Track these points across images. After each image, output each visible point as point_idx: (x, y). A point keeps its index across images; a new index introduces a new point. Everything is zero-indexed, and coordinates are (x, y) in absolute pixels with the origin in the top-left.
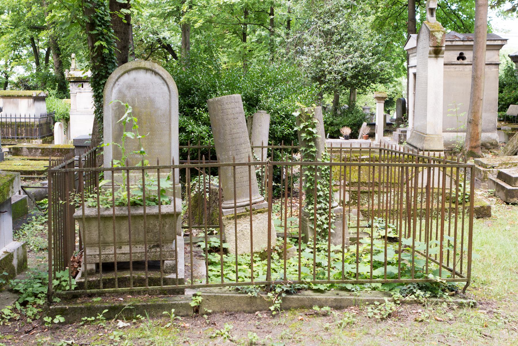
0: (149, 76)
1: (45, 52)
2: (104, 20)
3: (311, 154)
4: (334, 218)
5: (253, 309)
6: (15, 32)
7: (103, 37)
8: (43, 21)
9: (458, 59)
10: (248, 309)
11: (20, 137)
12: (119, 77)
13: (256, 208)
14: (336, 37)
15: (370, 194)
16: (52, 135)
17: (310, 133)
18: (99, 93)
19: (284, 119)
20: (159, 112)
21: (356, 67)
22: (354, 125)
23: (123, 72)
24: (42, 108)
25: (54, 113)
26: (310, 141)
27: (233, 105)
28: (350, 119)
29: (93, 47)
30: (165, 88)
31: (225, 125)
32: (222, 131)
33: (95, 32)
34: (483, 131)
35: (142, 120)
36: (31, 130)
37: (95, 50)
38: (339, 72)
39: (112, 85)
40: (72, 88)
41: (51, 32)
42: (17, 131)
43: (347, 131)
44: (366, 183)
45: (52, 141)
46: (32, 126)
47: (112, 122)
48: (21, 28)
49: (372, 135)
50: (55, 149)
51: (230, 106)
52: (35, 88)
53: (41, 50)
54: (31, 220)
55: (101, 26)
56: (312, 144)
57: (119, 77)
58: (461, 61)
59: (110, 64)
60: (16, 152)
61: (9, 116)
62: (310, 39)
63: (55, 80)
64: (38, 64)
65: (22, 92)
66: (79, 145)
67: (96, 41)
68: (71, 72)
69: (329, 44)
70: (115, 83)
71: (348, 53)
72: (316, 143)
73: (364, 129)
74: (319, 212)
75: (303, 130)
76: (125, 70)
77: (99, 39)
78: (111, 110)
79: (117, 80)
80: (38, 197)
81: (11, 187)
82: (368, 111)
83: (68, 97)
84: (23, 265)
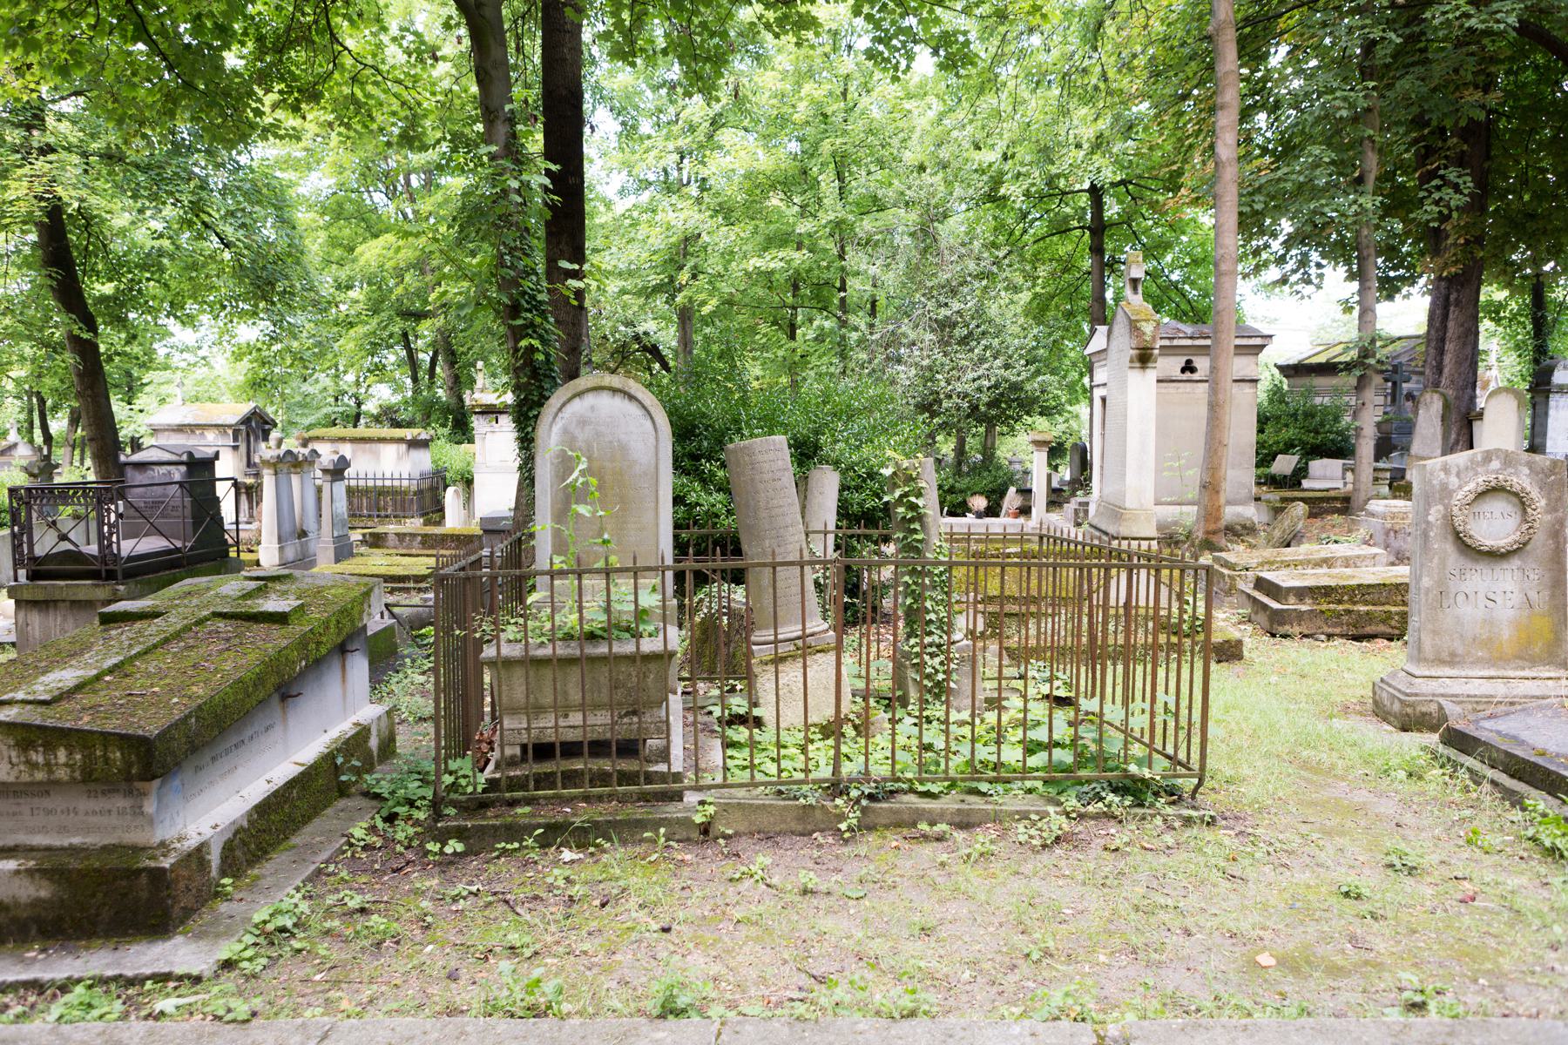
0: (619, 403)
6: (374, 322)
8: (426, 302)
9: (1183, 371)
10: (800, 828)
12: (564, 405)
14: (960, 332)
15: (1022, 618)
16: (442, 510)
17: (913, 507)
19: (864, 481)
21: (996, 386)
22: (993, 491)
24: (422, 461)
25: (446, 470)
26: (912, 520)
27: (771, 456)
28: (986, 481)
29: (516, 350)
30: (649, 424)
31: (757, 492)
33: (519, 322)
34: (1229, 503)
36: (403, 501)
38: (966, 395)
40: (478, 424)
41: (440, 321)
42: (378, 503)
43: (979, 503)
44: (1015, 599)
45: (441, 521)
49: (1025, 511)
51: (766, 457)
52: (410, 424)
53: (421, 356)
54: (403, 665)
56: (917, 526)
57: (564, 405)
58: (1188, 375)
60: (376, 541)
62: (912, 335)
63: (446, 410)
64: (415, 379)
67: (522, 338)
69: (948, 344)
71: (982, 360)
73: (1012, 499)
74: (929, 650)
75: (899, 501)
77: (528, 335)
79: (560, 409)
82: (1017, 467)
83: (471, 441)
84: (388, 748)
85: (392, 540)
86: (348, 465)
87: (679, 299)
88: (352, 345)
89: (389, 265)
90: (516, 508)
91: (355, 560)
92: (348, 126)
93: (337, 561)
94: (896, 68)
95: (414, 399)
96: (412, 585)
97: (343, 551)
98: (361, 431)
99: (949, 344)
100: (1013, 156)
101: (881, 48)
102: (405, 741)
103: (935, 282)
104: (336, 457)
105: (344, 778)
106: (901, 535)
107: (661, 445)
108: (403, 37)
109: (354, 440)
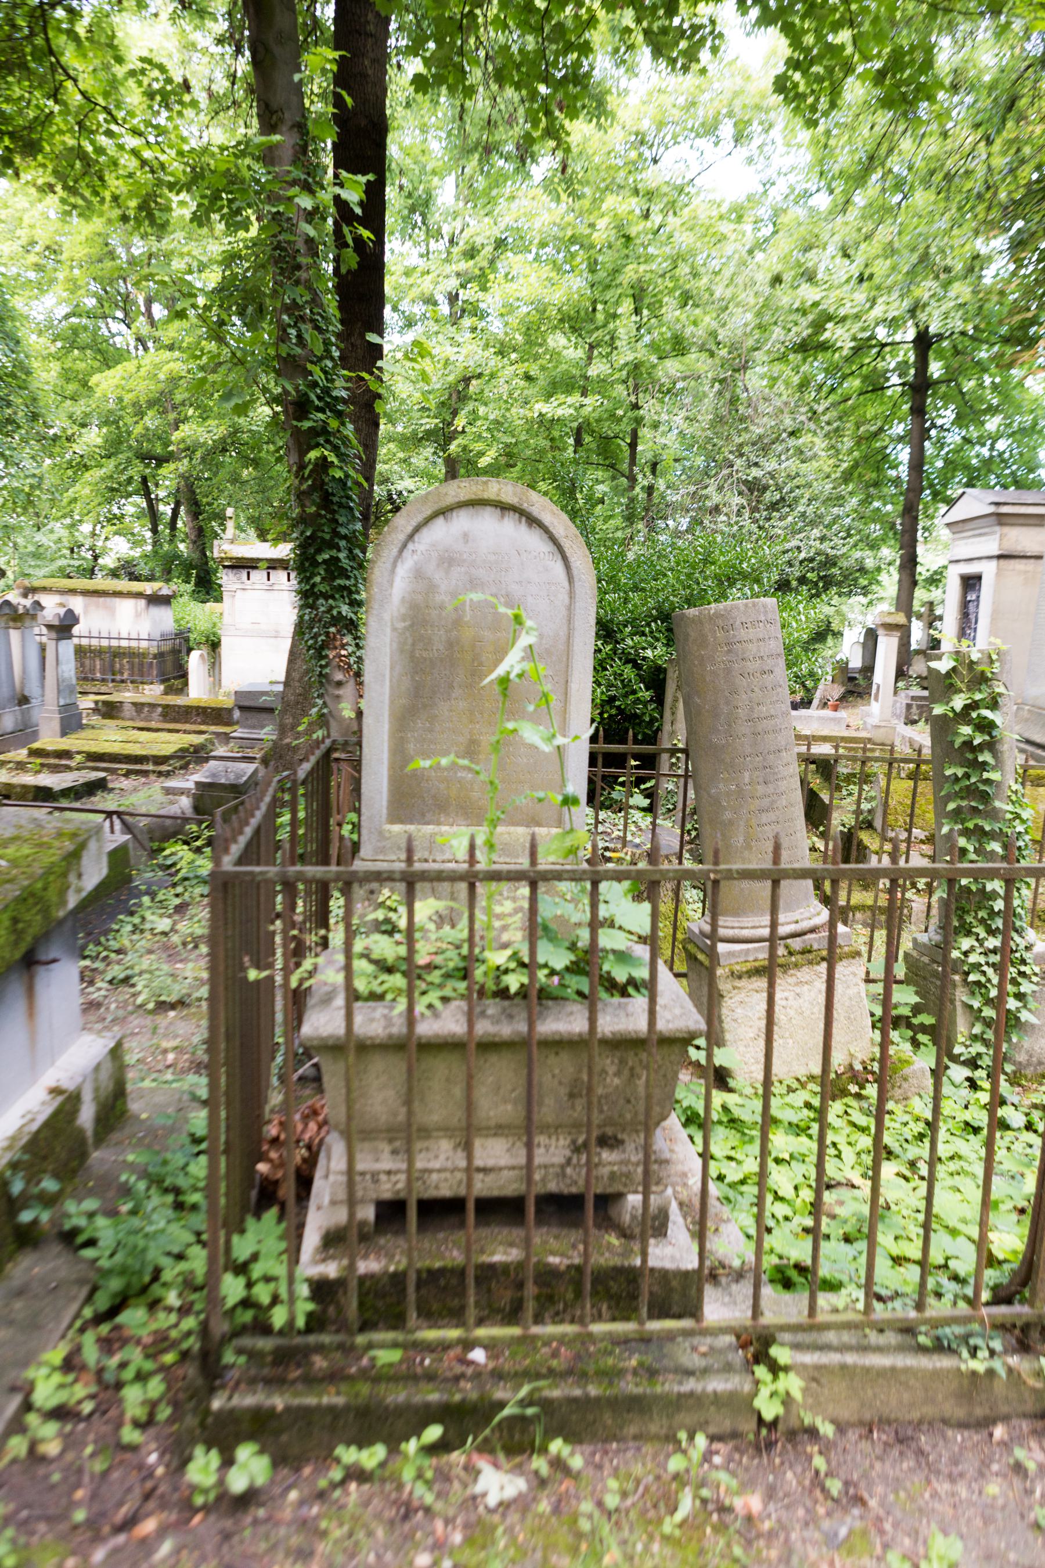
0: (511, 529)
1: (170, 512)
3: (982, 787)
4: (1035, 979)
5: (979, 1412)
6: (111, 463)
7: (327, 441)
8: (167, 444)
10: (960, 1413)
12: (417, 529)
13: (815, 947)
16: (184, 675)
17: (986, 726)
18: (314, 585)
23: (429, 512)
24: (164, 620)
25: (189, 630)
26: (981, 748)
27: (760, 631)
29: (302, 466)
30: (559, 567)
31: (735, 692)
32: (725, 710)
33: (306, 424)
35: (481, 664)
36: (141, 664)
37: (307, 472)
39: (395, 551)
40: (226, 579)
41: (183, 466)
42: (112, 666)
46: (143, 655)
47: (392, 668)
48: (122, 457)
51: (752, 633)
52: (151, 578)
53: (162, 508)
54: (140, 905)
55: (323, 411)
56: (985, 757)
57: (417, 529)
59: (342, 511)
60: (110, 710)
62: (716, 499)
63: (187, 567)
64: (154, 531)
65: (124, 584)
66: (246, 703)
67: (312, 448)
70: (404, 546)
72: (995, 756)
75: (964, 715)
76: (436, 507)
77: (318, 445)
78: (388, 630)
79: (411, 537)
80: (157, 834)
81: (72, 878)
83: (219, 599)
84: (113, 1109)
85: (128, 710)
86: (76, 620)
87: (453, 447)
88: (87, 491)
89: (128, 398)
90: (287, 684)
91: (83, 734)
92: (73, 191)
94: (813, 109)
95: (155, 552)
96: (150, 767)
97: (71, 723)
98: (100, 582)
99: (757, 510)
100: (871, 277)
101: (797, 76)
102: (151, 1094)
103: (745, 437)
104: (62, 611)
105: (26, 1217)
106: (960, 772)
109: (86, 593)
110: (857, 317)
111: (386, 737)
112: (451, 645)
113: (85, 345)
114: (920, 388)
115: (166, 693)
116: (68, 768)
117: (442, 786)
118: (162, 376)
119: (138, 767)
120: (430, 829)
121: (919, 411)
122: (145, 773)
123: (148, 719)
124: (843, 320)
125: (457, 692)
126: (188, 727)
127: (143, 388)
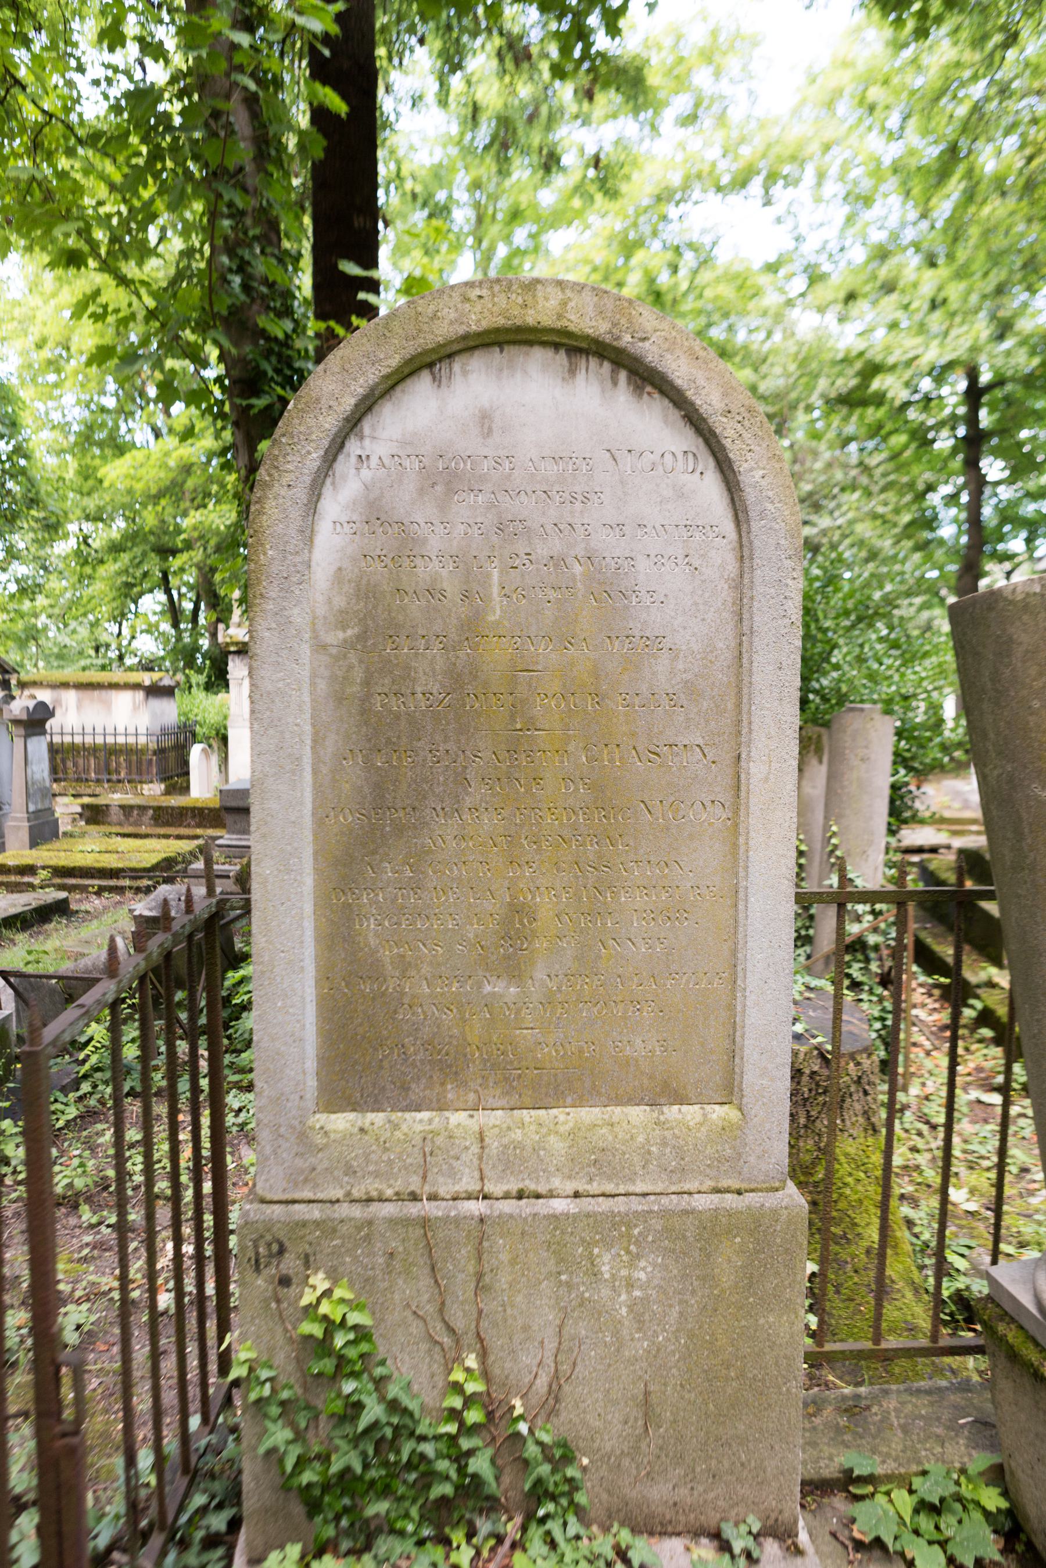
2: (290, 367)
11: (114, 777)
20: (662, 665)
23: (395, 362)
24: (168, 712)
30: (710, 488)
35: (531, 724)
36: (139, 762)
39: (314, 458)
41: (197, 555)
42: (107, 765)
45: (186, 789)
47: (317, 741)
50: (186, 809)
57: (368, 405)
60: (95, 815)
61: (89, 730)
68: (232, 631)
76: (411, 349)
78: (305, 650)
79: (353, 423)
85: (115, 814)
86: (51, 714)
89: (139, 486)
93: (34, 844)
96: (127, 882)
97: (44, 830)
100: (945, 301)
107: (763, 574)
108: (109, 81)
110: (909, 363)
111: (308, 908)
112: (457, 680)
113: (100, 439)
114: (974, 444)
115: (168, 792)
116: (31, 887)
117: (448, 1018)
118: (172, 463)
119: (112, 883)
120: (419, 1121)
121: (972, 465)
122: (120, 890)
123: (137, 824)
124: (893, 368)
125: (476, 794)
126: (182, 831)
127: (153, 477)
